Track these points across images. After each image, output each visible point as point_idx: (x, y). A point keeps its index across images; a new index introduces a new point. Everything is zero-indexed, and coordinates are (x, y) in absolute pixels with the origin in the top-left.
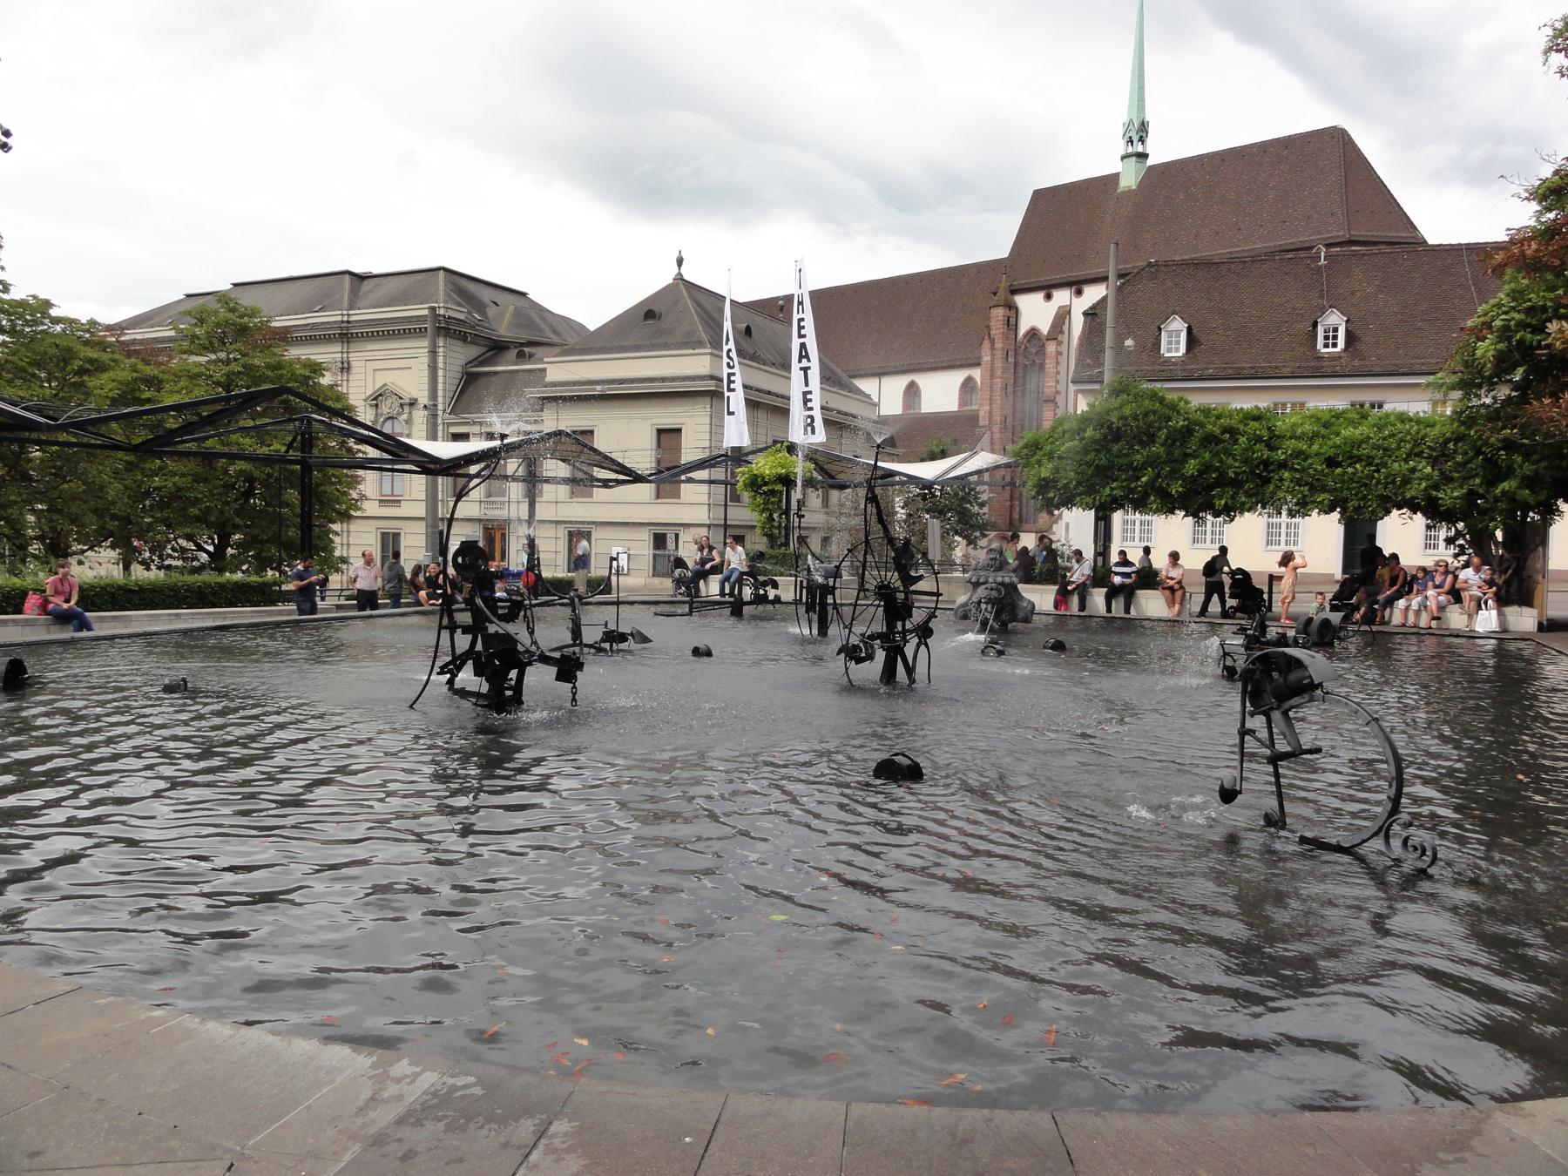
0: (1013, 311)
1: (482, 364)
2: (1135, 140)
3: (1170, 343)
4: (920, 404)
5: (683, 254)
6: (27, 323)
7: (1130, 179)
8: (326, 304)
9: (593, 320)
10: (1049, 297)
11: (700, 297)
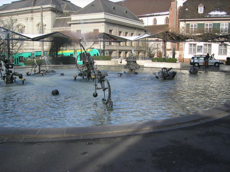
3: (200, 10)
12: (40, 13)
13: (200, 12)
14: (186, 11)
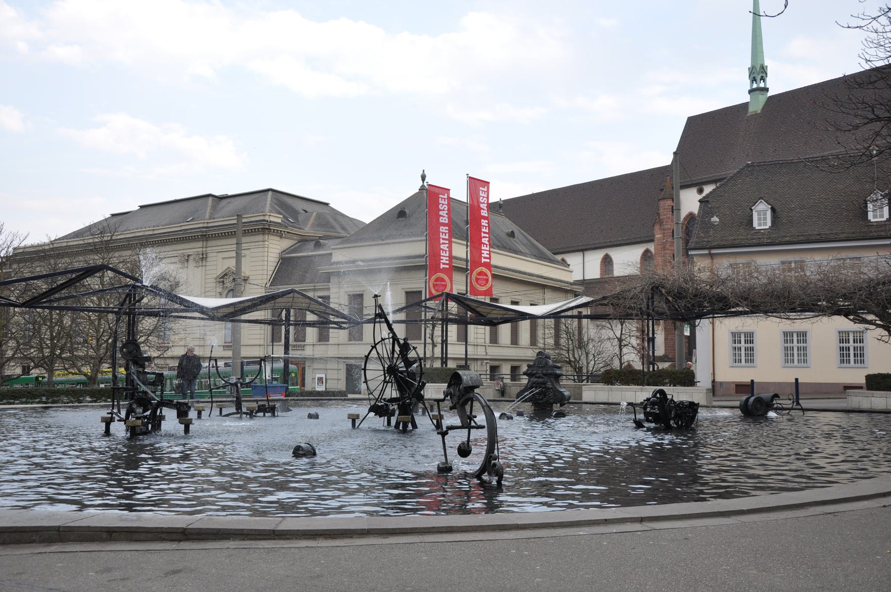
1: (295, 251)
2: (758, 78)
3: (759, 219)
4: (612, 271)
6: (686, 271)
7: (757, 107)
8: (195, 216)
9: (367, 218)
12: (234, 241)
13: (760, 225)
14: (712, 225)
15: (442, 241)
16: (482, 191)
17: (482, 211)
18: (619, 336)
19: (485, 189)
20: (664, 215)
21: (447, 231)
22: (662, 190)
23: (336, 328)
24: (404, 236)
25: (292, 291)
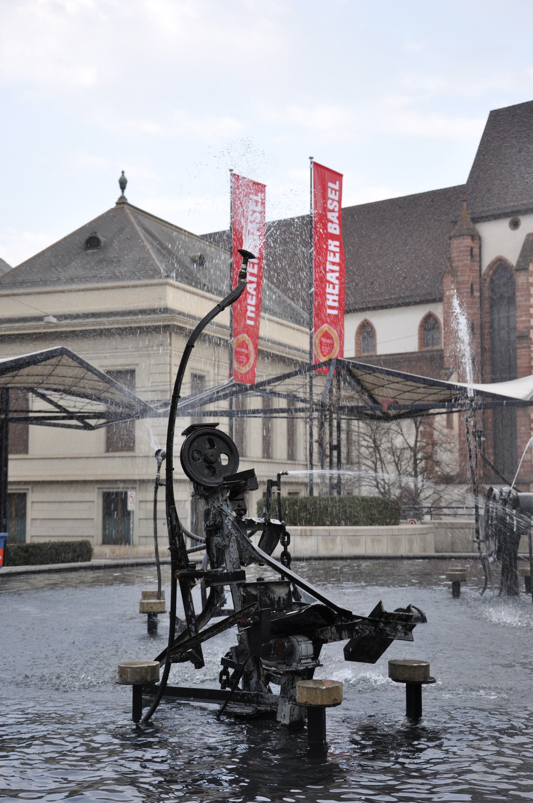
0: (477, 241)
5: (127, 176)
10: (515, 225)
11: (147, 223)
15: (329, 267)
16: (332, 189)
17: (330, 224)
18: (412, 444)
19: (337, 187)
20: (458, 261)
21: (338, 250)
22: (455, 223)
23: (77, 427)
24: (101, 279)
25: (63, 352)
